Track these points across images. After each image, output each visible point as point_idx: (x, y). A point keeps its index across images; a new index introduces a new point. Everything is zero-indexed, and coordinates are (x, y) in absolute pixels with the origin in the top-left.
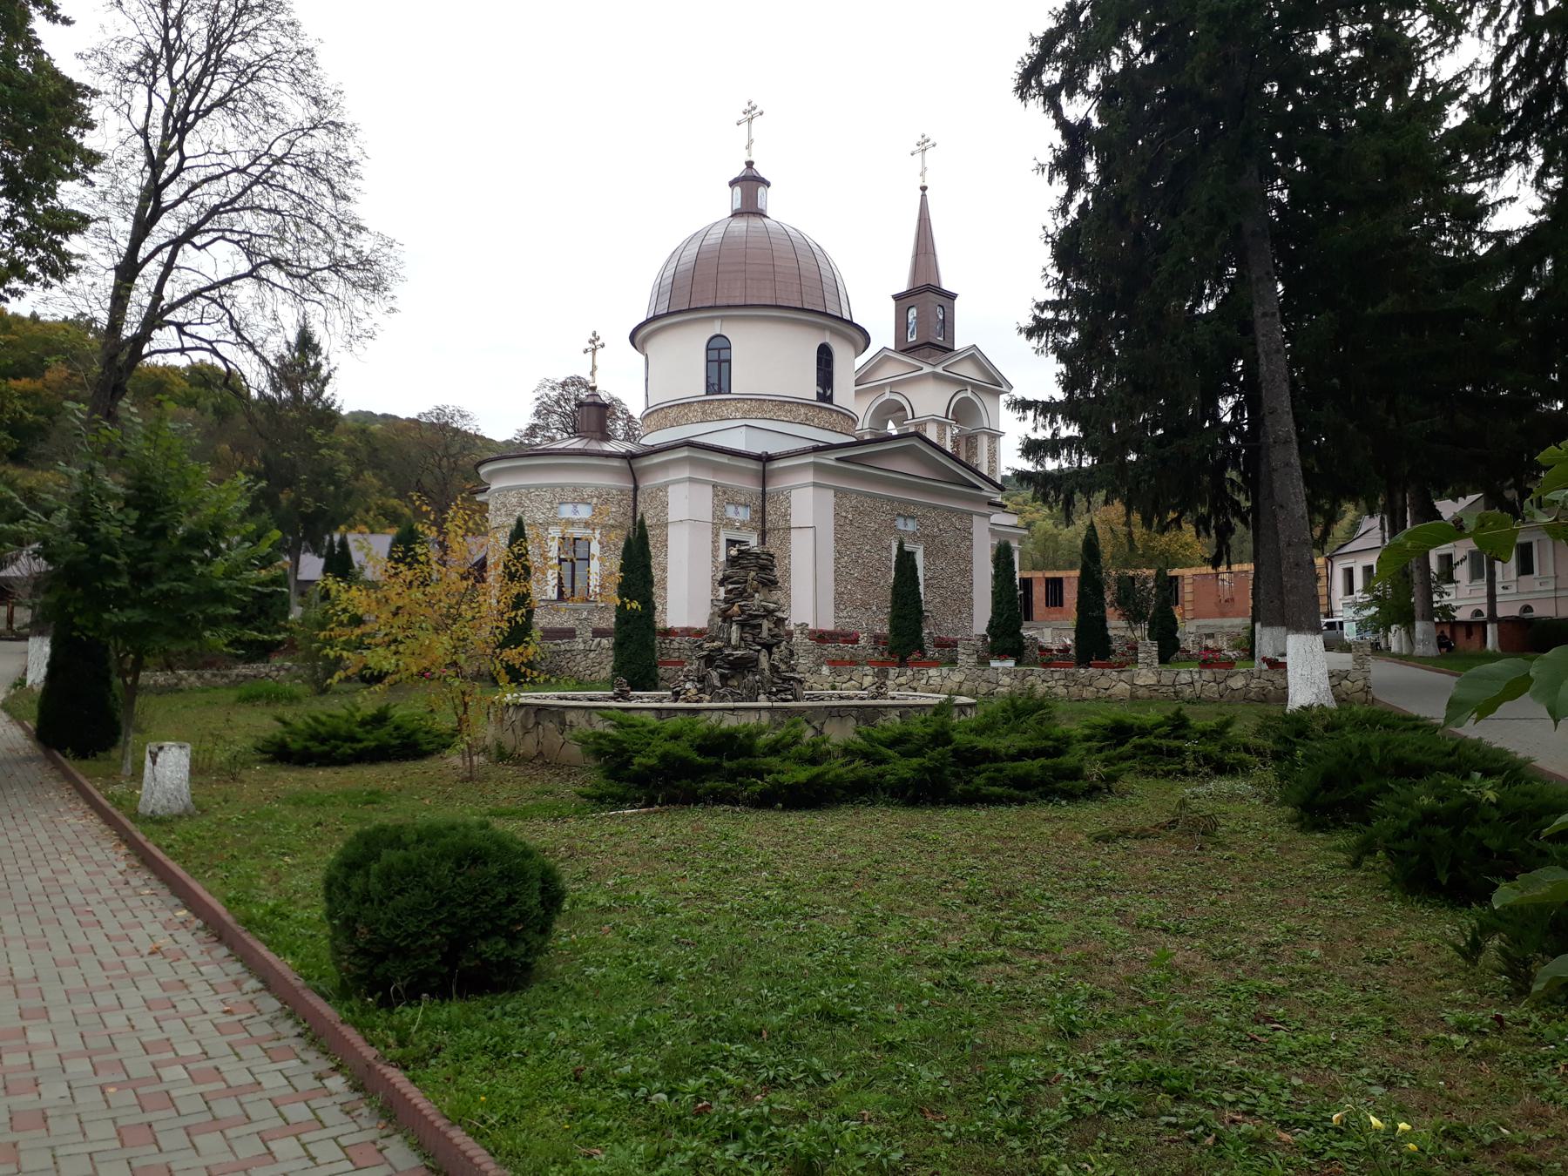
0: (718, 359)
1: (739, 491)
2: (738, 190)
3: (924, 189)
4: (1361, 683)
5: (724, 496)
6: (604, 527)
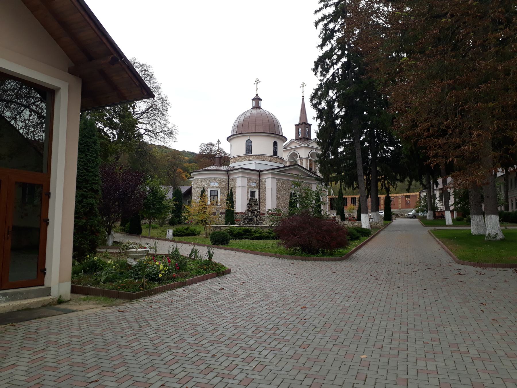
0: (249, 148)
1: (254, 179)
2: (254, 102)
3: (303, 97)
5: (250, 180)
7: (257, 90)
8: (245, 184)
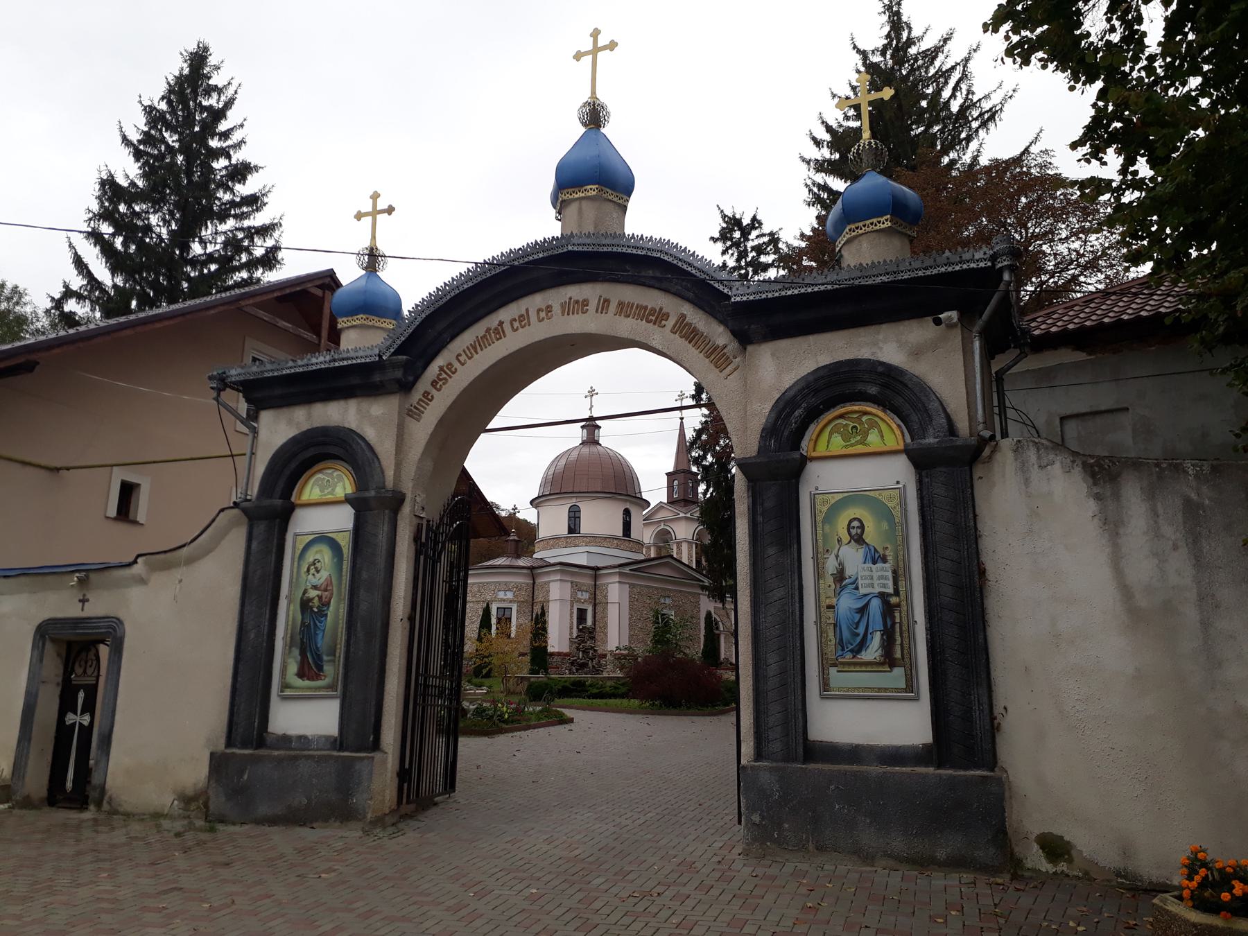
5: (576, 587)
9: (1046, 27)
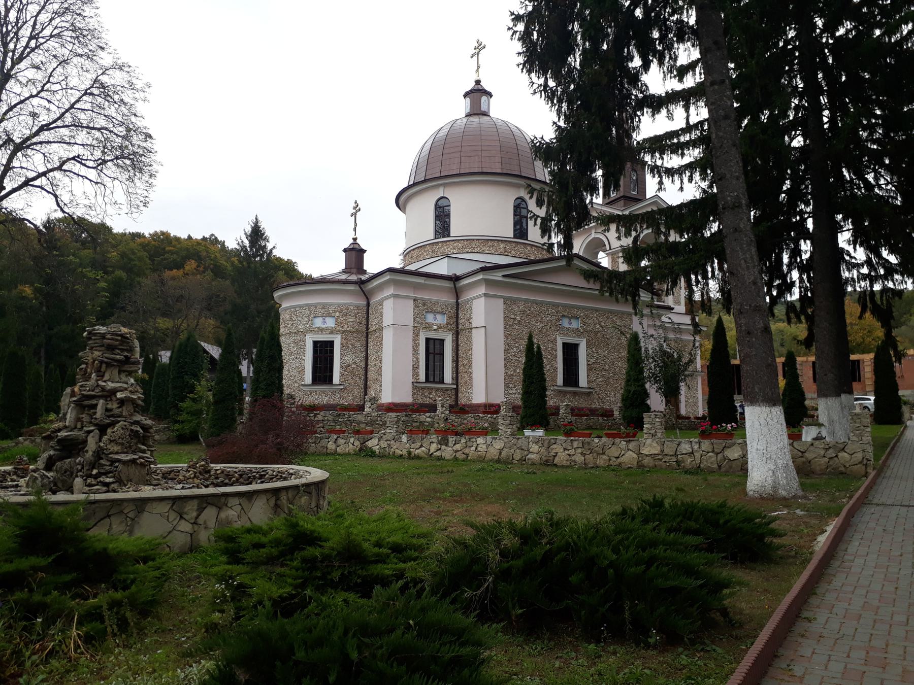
1: (436, 303)
2: (468, 99)
4: (859, 456)
5: (422, 307)
6: (344, 332)
7: (477, 71)
8: (408, 317)
9: (844, 170)
